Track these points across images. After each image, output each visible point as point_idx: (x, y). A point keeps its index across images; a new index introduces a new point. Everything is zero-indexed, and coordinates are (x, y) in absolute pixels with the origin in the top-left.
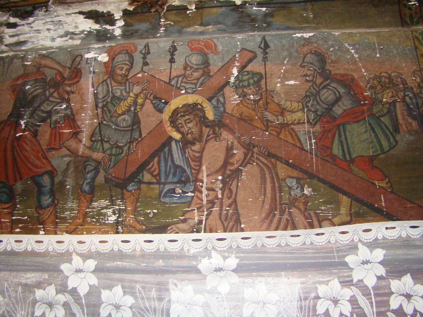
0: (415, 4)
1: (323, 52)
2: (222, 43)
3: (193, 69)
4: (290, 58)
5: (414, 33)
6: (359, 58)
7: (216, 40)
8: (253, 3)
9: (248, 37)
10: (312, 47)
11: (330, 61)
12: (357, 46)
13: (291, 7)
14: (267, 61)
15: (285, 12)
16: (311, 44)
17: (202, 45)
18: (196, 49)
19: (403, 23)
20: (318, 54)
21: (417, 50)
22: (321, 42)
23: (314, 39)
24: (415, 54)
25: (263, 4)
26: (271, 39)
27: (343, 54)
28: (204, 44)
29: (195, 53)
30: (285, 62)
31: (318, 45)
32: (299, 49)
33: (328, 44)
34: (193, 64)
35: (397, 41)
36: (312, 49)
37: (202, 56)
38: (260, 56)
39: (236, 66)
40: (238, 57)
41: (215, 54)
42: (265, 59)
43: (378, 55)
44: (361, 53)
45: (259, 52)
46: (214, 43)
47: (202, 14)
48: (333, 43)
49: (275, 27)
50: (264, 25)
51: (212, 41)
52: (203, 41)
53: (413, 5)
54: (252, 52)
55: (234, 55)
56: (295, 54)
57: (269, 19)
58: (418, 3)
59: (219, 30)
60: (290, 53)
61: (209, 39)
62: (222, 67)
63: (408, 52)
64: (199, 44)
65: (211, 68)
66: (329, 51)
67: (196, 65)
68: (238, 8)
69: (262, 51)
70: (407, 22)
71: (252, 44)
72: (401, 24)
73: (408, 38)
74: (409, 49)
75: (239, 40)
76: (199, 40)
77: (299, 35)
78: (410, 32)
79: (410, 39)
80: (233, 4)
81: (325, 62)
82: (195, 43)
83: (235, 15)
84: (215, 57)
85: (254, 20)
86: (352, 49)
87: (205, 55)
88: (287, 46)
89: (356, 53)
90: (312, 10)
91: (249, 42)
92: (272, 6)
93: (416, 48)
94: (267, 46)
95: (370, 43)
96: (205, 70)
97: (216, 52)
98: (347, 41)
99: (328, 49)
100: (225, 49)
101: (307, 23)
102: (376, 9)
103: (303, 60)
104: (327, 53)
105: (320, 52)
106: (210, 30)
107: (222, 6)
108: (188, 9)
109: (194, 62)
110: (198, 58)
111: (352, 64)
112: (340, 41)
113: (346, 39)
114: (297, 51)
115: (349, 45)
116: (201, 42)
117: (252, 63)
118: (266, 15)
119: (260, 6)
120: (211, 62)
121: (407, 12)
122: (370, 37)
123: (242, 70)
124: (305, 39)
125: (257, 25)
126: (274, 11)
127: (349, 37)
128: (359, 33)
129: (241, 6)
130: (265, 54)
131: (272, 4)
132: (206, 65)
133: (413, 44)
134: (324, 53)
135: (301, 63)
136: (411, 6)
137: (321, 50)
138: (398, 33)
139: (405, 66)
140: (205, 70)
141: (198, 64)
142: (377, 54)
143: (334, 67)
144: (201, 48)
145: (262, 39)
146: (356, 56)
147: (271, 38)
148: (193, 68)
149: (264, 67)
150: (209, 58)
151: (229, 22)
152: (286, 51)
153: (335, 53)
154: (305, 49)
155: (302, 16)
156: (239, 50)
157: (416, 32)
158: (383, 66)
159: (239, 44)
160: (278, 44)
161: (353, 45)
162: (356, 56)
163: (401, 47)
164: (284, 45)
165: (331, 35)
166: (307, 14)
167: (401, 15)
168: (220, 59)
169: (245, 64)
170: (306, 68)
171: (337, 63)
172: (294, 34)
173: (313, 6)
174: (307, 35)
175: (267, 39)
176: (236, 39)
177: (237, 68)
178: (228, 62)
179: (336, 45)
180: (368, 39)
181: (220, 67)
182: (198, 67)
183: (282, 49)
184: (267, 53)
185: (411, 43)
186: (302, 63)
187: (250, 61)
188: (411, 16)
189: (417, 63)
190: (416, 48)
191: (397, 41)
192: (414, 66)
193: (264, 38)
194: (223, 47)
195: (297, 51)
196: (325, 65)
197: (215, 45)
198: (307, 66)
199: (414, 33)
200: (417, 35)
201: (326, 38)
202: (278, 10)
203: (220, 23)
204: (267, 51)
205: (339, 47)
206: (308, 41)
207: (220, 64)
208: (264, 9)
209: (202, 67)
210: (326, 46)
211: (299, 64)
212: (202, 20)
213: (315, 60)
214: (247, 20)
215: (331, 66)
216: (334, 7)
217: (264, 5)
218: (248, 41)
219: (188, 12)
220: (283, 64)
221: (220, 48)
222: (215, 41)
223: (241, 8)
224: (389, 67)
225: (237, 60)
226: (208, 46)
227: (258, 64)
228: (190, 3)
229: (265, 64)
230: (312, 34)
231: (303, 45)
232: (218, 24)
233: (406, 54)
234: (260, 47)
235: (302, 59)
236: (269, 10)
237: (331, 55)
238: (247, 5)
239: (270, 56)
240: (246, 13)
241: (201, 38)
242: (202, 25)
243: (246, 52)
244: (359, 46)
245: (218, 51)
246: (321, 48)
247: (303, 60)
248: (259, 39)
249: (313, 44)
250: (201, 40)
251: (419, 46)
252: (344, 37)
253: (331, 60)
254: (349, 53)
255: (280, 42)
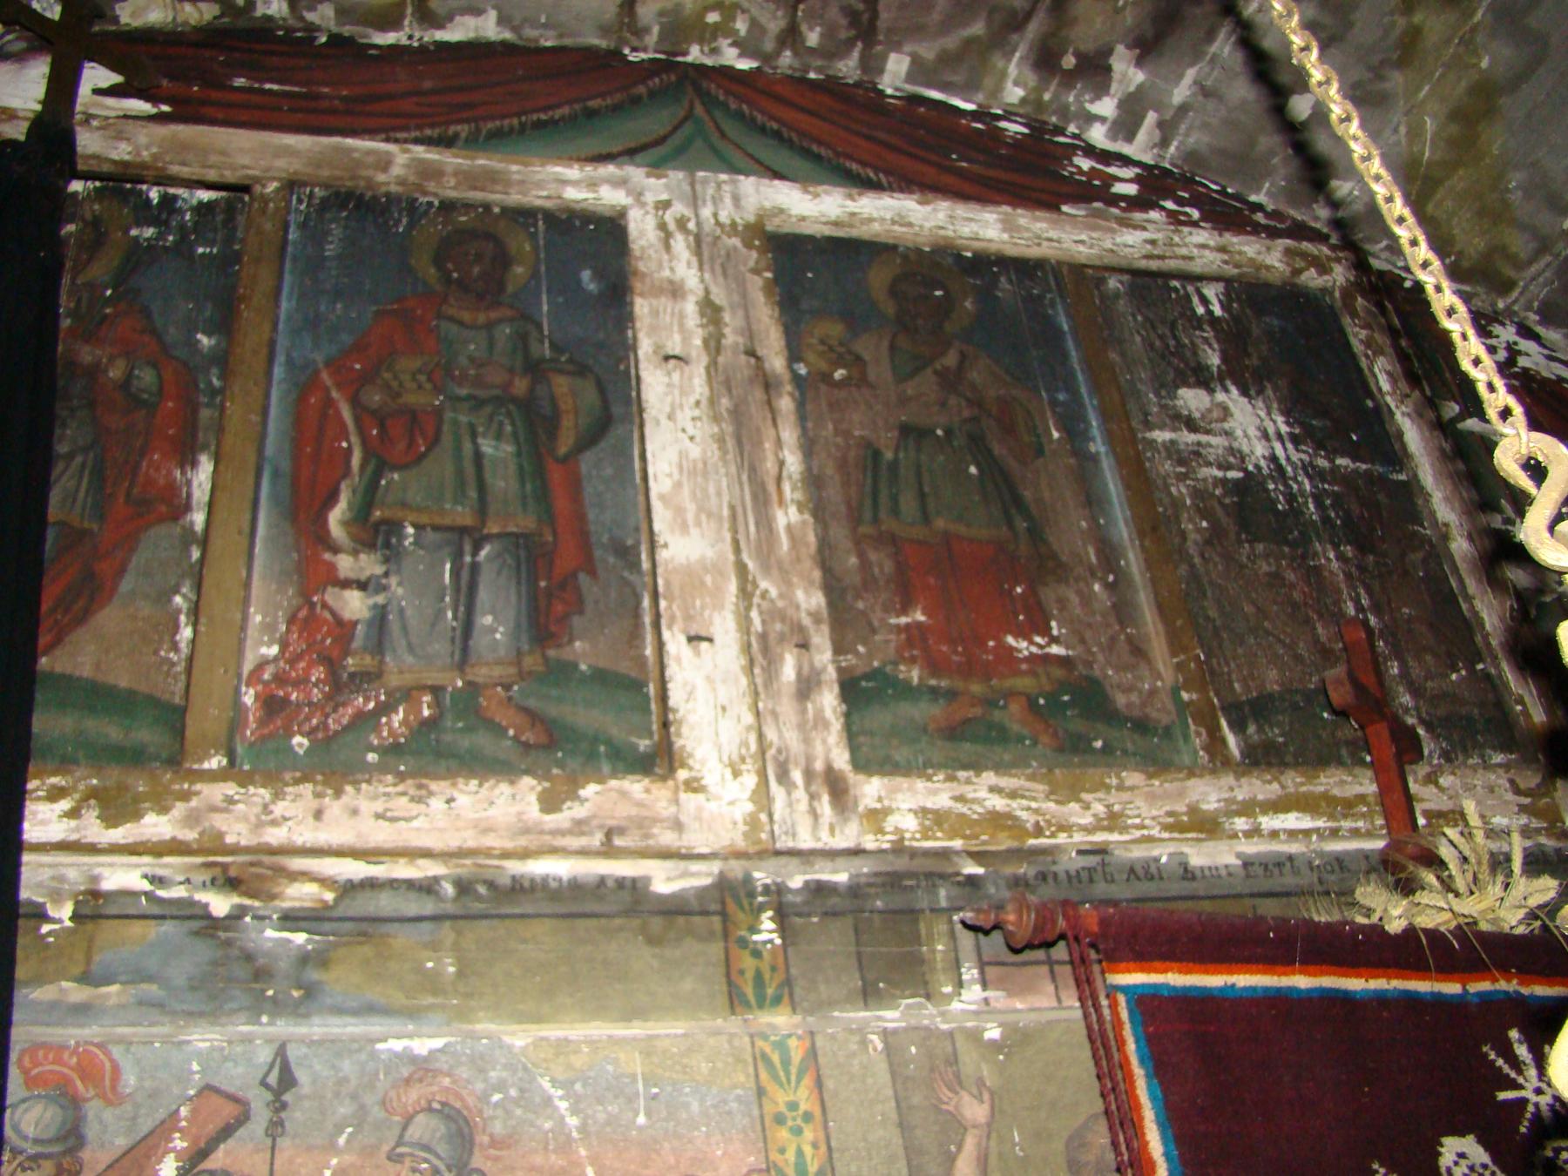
0: (771, 941)
1: (467, 1108)
2: (138, 1062)
3: (20, 1158)
4: (359, 1127)
5: (760, 1043)
6: (583, 1129)
7: (121, 1048)
8: (266, 913)
9: (230, 1042)
10: (435, 1088)
11: (486, 1139)
12: (578, 1086)
13: (388, 935)
14: (282, 1135)
15: (367, 950)
16: (434, 1077)
17: (71, 1068)
18: (46, 1083)
19: (735, 1001)
20: (453, 1113)
21: (764, 1100)
22: (464, 1072)
23: (444, 1058)
24: (756, 1112)
25: (305, 919)
26: (306, 1056)
27: (530, 1116)
28: (79, 1063)
29: (39, 1096)
30: (342, 1140)
31: (454, 1082)
32: (393, 1094)
33: (485, 1080)
34: (26, 1138)
35: (705, 1067)
36: (433, 1094)
37: (62, 1107)
38: (261, 1115)
39: (174, 1150)
40: (186, 1119)
41: (109, 1103)
42: (276, 1128)
43: (641, 1119)
44: (590, 1112)
45: (259, 1102)
46: (112, 1061)
47: (91, 940)
48: (504, 1074)
49: (329, 1001)
50: (296, 994)
51: (108, 1054)
52: (75, 1052)
53: (765, 942)
54: (235, 1099)
55: (174, 1107)
56: (377, 1113)
57: (314, 975)
58: (783, 938)
59: (140, 1003)
60: (362, 1107)
61: (98, 1045)
62: (124, 1154)
63: (734, 1105)
64: (59, 1061)
65: (86, 1155)
66: (488, 1103)
67: (37, 1141)
68: (216, 928)
69: (269, 1096)
70: (744, 995)
71: (240, 1070)
72: (727, 1002)
73: (739, 1060)
74: (738, 1099)
75: (199, 1055)
76: (63, 1048)
77: (397, 1045)
78: (747, 1039)
79: (744, 1062)
80: (201, 912)
81: (472, 1143)
82: (46, 1057)
83: (203, 951)
84: (108, 1115)
85: (262, 974)
86: (561, 1098)
87: (73, 1103)
88: (354, 1082)
89: (574, 1111)
90: (457, 948)
91: (230, 1064)
92: (327, 926)
93: (761, 1092)
94: (288, 1079)
95: (623, 1075)
96: (66, 1161)
97: (112, 1095)
98: (547, 1069)
99: (484, 1098)
100: (147, 1084)
101: (435, 993)
102: (657, 950)
103: (401, 1136)
104: (480, 1112)
105: (458, 1105)
106: (113, 1001)
107: (163, 917)
108: (43, 917)
109: (31, 1131)
110: (48, 1114)
111: (554, 1151)
112: (525, 1069)
113: (545, 1060)
114: (383, 1103)
115: (553, 1081)
116: (66, 1056)
117: (231, 1142)
118: (305, 959)
119: (289, 924)
120: (91, 1131)
121: (748, 963)
122: (622, 1056)
123: (193, 1166)
124: (413, 1059)
125: (270, 993)
126: (336, 945)
127: (557, 1055)
128: (590, 1042)
129: (227, 922)
130: (277, 1111)
131: (331, 919)
132: (71, 1142)
133: (752, 1079)
134: (470, 1111)
135: (392, 1144)
136: (759, 947)
137: (462, 1100)
138: (712, 1041)
139: (724, 1154)
140: (66, 1161)
141: (45, 1136)
142: (637, 1114)
143: (497, 1159)
144: (64, 1075)
145: (277, 1054)
146: (573, 1121)
147: (304, 1050)
148: (21, 1153)
149: (269, 1155)
150: (85, 1117)
151: (180, 972)
152: (347, 1101)
153: (507, 1112)
154: (413, 1095)
155: (420, 969)
156: (192, 1092)
157: (765, 1037)
158: (654, 1156)
159: (195, 1067)
160: (325, 1073)
161: (567, 1085)
162: (573, 1121)
163: (714, 1090)
164: (346, 1080)
165: (501, 1047)
166: (438, 961)
167: (728, 975)
168: (122, 1123)
169: (207, 1143)
170: (408, 1162)
171: (509, 1147)
172: (380, 1041)
173: (459, 933)
174: (422, 1046)
175: (293, 1053)
176: (189, 1048)
177: (177, 1159)
178: (151, 1133)
179: (513, 1085)
180: (616, 1062)
181: (119, 1152)
182: (39, 1149)
183: (337, 1095)
184: (284, 1106)
185: (748, 1076)
186: (398, 1144)
187: (227, 1132)
188: (759, 980)
189: (761, 1145)
190: (761, 1092)
191: (705, 1067)
192: (749, 1155)
193: (281, 1052)
194: (141, 1079)
195: (383, 1103)
196: (471, 1153)
197: (116, 1069)
198: (411, 1155)
199: (760, 1043)
200: (768, 1050)
201: (482, 1057)
202: (345, 944)
203: (150, 979)
204: (287, 1097)
205: (522, 1090)
206: (422, 1068)
207: (122, 1142)
208: (300, 938)
209: (56, 1149)
210: (479, 1086)
211: (386, 1148)
212: (89, 960)
213: (438, 1135)
214: (241, 971)
215: (488, 1158)
216: (524, 941)
217: (303, 924)
218: (226, 1059)
219: (45, 928)
220: (331, 1148)
221: (130, 1080)
222: (117, 1052)
223: (226, 929)
224: (672, 1161)
225: (181, 1130)
226: (89, 1070)
227: (250, 1146)
228: (57, 897)
229: (273, 1148)
230: (438, 1043)
231: (408, 1081)
232: (142, 981)
233: (729, 1113)
234: (264, 1083)
235: (396, 1131)
236: (317, 942)
237: (493, 1118)
238: (248, 919)
239: (296, 1116)
240: (242, 949)
241: (71, 1036)
242: (86, 978)
243: (217, 1100)
244: (584, 1086)
245: (120, 1089)
246: (464, 1093)
247: (401, 1136)
248: (264, 1055)
249: (439, 1079)
250: (67, 1047)
251: (770, 1087)
252: (542, 1055)
253: (491, 1136)
254: (549, 1111)
255: (333, 1067)
